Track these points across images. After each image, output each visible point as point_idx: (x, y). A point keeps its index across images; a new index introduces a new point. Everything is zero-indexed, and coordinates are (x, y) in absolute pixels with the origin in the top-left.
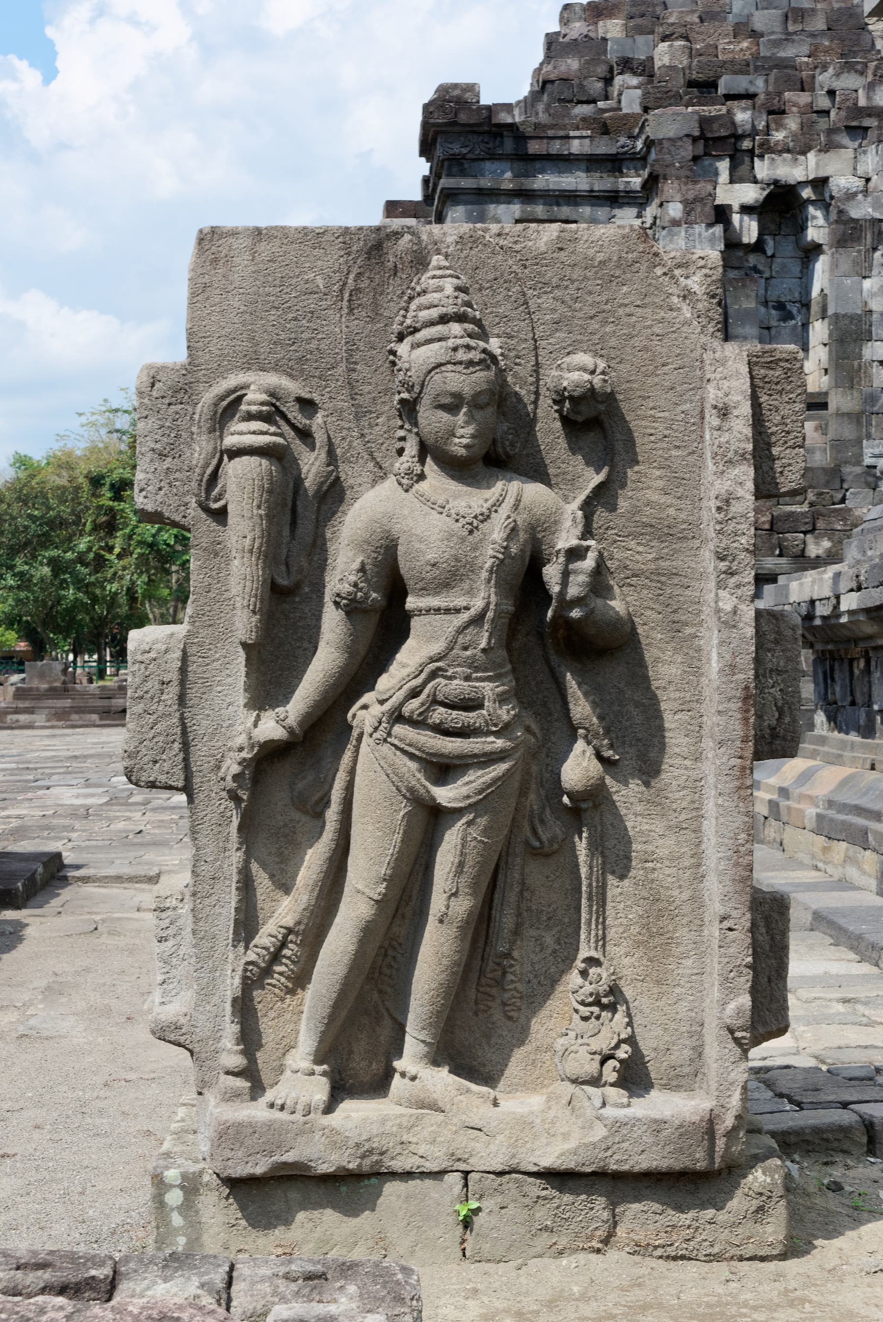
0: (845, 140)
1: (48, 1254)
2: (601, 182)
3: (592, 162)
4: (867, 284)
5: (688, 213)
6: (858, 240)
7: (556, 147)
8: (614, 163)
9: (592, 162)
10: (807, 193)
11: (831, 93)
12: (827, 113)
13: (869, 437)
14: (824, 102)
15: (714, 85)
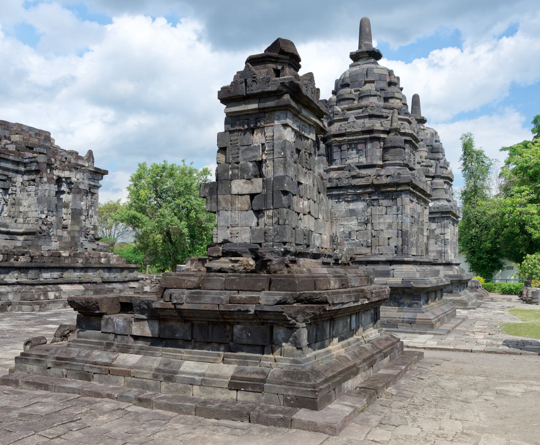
0: (73, 170)
1: (242, 404)
2: (15, 167)
3: (13, 162)
4: (82, 203)
5: (48, 181)
6: (81, 193)
7: (6, 157)
8: (18, 163)
9: (13, 162)
10: (64, 180)
11: (66, 158)
12: (64, 162)
13: (81, 236)
14: (64, 160)
15: (33, 149)
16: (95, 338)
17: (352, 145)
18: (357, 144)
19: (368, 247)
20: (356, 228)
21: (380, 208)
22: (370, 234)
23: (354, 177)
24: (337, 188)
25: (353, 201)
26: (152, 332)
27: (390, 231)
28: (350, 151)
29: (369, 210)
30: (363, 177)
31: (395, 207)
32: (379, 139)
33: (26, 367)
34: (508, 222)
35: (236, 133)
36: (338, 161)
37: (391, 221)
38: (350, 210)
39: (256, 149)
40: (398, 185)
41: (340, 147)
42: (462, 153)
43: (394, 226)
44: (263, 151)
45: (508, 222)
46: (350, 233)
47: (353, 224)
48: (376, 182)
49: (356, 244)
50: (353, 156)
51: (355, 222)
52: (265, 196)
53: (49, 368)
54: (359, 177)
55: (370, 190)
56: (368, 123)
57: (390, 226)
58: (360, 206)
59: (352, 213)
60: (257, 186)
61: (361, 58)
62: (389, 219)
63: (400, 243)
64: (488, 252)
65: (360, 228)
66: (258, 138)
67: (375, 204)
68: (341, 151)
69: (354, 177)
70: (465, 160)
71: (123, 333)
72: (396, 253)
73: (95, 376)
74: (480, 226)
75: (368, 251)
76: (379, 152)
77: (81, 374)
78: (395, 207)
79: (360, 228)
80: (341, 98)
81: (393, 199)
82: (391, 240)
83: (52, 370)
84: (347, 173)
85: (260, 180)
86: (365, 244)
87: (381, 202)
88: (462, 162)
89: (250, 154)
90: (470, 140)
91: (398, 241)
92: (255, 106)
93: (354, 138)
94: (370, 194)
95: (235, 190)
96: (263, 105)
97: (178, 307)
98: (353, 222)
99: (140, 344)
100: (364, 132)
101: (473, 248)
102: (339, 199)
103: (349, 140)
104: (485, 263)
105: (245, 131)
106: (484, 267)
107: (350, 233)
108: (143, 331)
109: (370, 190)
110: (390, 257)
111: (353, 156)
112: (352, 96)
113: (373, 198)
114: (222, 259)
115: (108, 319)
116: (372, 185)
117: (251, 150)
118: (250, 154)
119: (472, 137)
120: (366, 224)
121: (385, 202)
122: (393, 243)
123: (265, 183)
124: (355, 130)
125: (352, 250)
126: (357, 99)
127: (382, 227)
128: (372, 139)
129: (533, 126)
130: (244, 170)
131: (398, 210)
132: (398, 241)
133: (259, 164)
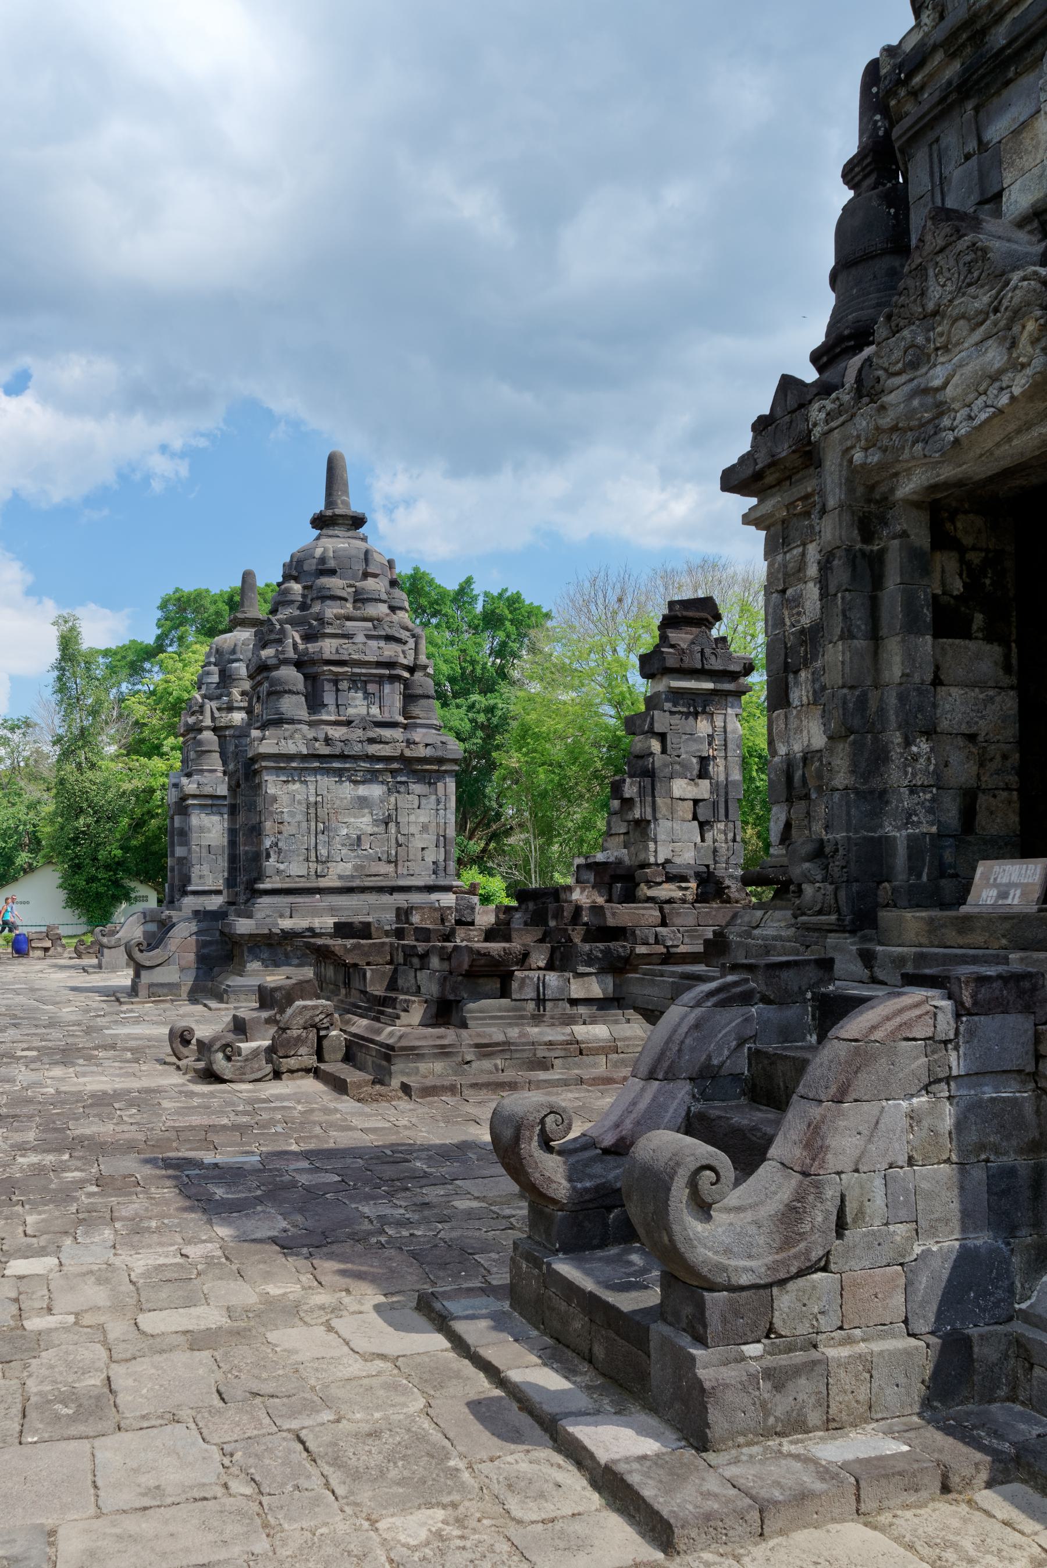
16: (500, 1010)
17: (358, 682)
18: (366, 682)
19: (390, 862)
20: (370, 830)
21: (410, 797)
22: (394, 841)
23: (372, 741)
24: (342, 757)
25: (363, 782)
26: (604, 991)
27: (425, 836)
28: (352, 694)
29: (392, 799)
30: (387, 743)
31: (434, 797)
32: (398, 678)
33: (417, 1068)
34: (159, 807)
35: (677, 716)
36: (332, 708)
37: (426, 820)
38: (359, 797)
39: (700, 740)
40: (441, 761)
41: (336, 682)
42: (57, 655)
43: (432, 828)
44: (710, 744)
45: (159, 807)
46: (359, 838)
47: (364, 822)
48: (408, 753)
49: (369, 858)
50: (358, 702)
51: (367, 819)
52: (715, 805)
53: (468, 1063)
54: (381, 742)
55: (395, 766)
56: (390, 651)
57: (425, 828)
58: (375, 791)
59: (363, 802)
60: (703, 789)
61: (338, 524)
62: (423, 817)
63: (442, 858)
64: (107, 867)
65: (376, 829)
66: (703, 727)
67: (402, 789)
68: (338, 690)
69: (372, 741)
70: (62, 669)
71: (558, 996)
72: (434, 873)
73: (556, 1062)
74: (95, 813)
75: (391, 868)
76: (398, 702)
77: (531, 1062)
78: (434, 797)
79: (376, 829)
80: (328, 593)
81: (430, 784)
82: (426, 852)
83: (474, 1065)
84: (360, 732)
85: (707, 782)
86: (384, 857)
87: (412, 786)
88: (56, 673)
89: (694, 747)
90: (72, 629)
91: (438, 853)
92: (710, 686)
93: (364, 671)
94: (393, 772)
95: (677, 793)
96: (720, 686)
97: (673, 950)
98: (364, 819)
99: (582, 1010)
100: (379, 664)
101: (77, 856)
102: (341, 776)
103: (354, 674)
104: (102, 890)
105: (687, 715)
106: (98, 896)
107: (359, 838)
108: (588, 990)
109: (395, 766)
110: (430, 880)
111: (358, 702)
112: (345, 595)
113: (399, 779)
114: (665, 886)
115: (523, 979)
116: (402, 758)
117: (695, 740)
118: (694, 747)
119: (77, 623)
120: (387, 824)
121: (417, 788)
122: (430, 857)
123: (715, 788)
124: (367, 658)
125: (362, 867)
126: (351, 600)
127: (413, 829)
128: (394, 679)
129: (159, 614)
130: (685, 766)
131: (438, 802)
132: (438, 853)
133: (704, 761)
